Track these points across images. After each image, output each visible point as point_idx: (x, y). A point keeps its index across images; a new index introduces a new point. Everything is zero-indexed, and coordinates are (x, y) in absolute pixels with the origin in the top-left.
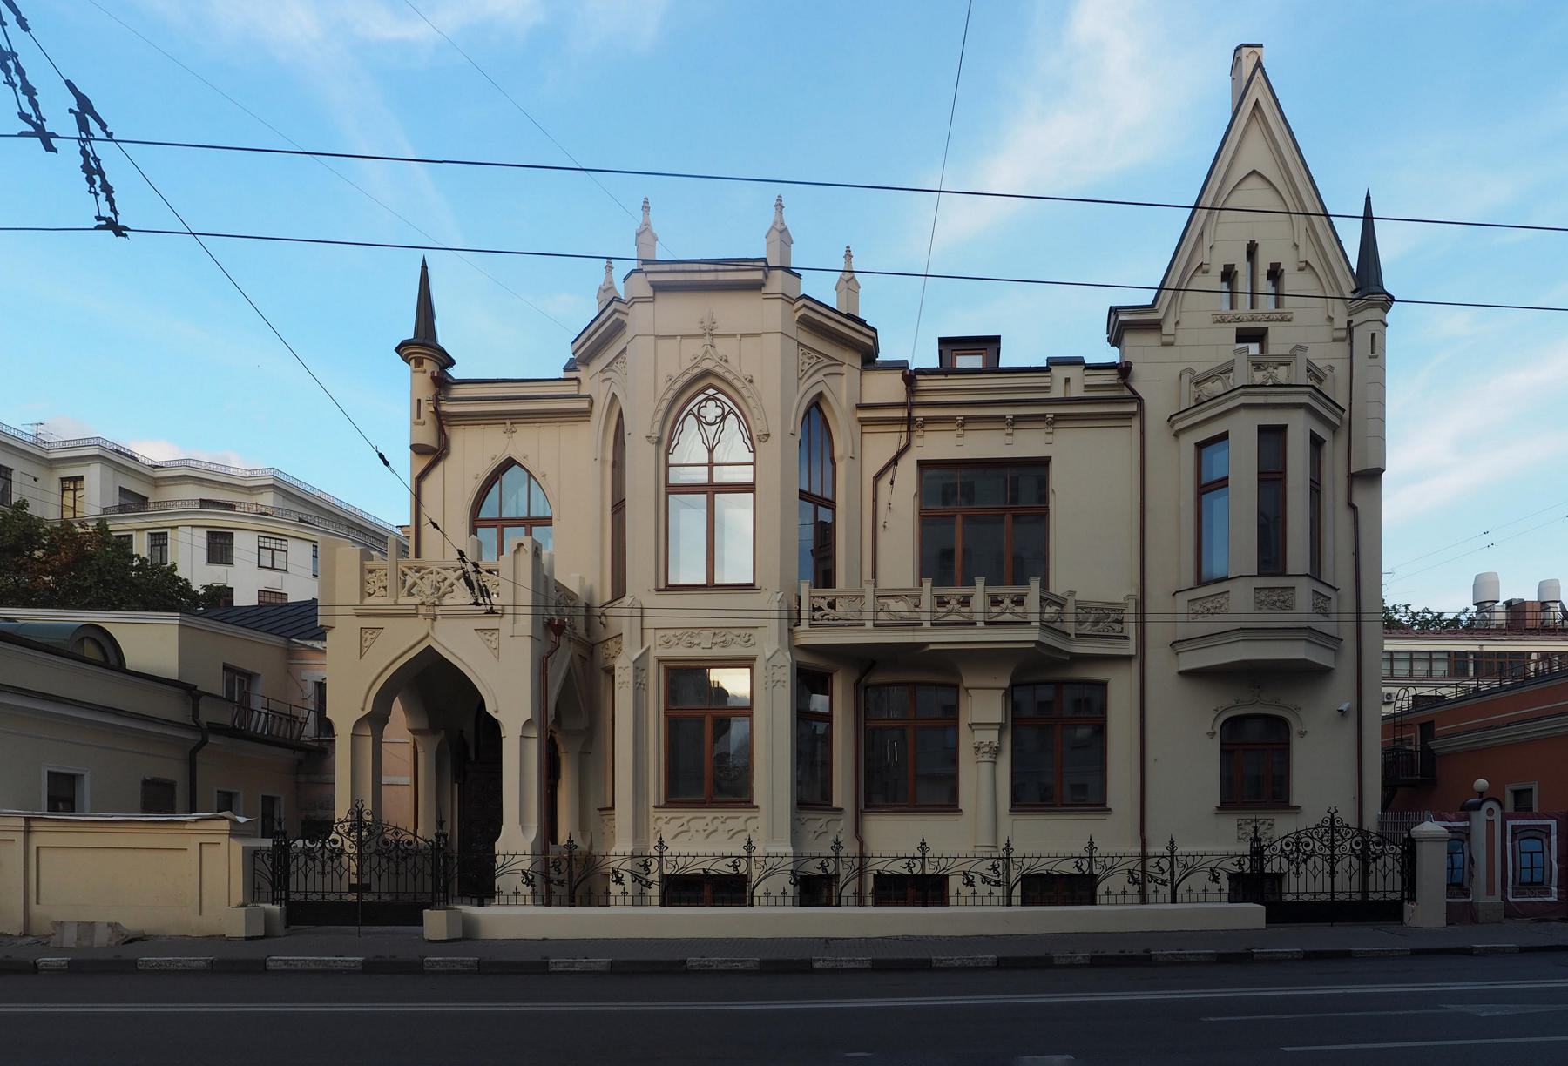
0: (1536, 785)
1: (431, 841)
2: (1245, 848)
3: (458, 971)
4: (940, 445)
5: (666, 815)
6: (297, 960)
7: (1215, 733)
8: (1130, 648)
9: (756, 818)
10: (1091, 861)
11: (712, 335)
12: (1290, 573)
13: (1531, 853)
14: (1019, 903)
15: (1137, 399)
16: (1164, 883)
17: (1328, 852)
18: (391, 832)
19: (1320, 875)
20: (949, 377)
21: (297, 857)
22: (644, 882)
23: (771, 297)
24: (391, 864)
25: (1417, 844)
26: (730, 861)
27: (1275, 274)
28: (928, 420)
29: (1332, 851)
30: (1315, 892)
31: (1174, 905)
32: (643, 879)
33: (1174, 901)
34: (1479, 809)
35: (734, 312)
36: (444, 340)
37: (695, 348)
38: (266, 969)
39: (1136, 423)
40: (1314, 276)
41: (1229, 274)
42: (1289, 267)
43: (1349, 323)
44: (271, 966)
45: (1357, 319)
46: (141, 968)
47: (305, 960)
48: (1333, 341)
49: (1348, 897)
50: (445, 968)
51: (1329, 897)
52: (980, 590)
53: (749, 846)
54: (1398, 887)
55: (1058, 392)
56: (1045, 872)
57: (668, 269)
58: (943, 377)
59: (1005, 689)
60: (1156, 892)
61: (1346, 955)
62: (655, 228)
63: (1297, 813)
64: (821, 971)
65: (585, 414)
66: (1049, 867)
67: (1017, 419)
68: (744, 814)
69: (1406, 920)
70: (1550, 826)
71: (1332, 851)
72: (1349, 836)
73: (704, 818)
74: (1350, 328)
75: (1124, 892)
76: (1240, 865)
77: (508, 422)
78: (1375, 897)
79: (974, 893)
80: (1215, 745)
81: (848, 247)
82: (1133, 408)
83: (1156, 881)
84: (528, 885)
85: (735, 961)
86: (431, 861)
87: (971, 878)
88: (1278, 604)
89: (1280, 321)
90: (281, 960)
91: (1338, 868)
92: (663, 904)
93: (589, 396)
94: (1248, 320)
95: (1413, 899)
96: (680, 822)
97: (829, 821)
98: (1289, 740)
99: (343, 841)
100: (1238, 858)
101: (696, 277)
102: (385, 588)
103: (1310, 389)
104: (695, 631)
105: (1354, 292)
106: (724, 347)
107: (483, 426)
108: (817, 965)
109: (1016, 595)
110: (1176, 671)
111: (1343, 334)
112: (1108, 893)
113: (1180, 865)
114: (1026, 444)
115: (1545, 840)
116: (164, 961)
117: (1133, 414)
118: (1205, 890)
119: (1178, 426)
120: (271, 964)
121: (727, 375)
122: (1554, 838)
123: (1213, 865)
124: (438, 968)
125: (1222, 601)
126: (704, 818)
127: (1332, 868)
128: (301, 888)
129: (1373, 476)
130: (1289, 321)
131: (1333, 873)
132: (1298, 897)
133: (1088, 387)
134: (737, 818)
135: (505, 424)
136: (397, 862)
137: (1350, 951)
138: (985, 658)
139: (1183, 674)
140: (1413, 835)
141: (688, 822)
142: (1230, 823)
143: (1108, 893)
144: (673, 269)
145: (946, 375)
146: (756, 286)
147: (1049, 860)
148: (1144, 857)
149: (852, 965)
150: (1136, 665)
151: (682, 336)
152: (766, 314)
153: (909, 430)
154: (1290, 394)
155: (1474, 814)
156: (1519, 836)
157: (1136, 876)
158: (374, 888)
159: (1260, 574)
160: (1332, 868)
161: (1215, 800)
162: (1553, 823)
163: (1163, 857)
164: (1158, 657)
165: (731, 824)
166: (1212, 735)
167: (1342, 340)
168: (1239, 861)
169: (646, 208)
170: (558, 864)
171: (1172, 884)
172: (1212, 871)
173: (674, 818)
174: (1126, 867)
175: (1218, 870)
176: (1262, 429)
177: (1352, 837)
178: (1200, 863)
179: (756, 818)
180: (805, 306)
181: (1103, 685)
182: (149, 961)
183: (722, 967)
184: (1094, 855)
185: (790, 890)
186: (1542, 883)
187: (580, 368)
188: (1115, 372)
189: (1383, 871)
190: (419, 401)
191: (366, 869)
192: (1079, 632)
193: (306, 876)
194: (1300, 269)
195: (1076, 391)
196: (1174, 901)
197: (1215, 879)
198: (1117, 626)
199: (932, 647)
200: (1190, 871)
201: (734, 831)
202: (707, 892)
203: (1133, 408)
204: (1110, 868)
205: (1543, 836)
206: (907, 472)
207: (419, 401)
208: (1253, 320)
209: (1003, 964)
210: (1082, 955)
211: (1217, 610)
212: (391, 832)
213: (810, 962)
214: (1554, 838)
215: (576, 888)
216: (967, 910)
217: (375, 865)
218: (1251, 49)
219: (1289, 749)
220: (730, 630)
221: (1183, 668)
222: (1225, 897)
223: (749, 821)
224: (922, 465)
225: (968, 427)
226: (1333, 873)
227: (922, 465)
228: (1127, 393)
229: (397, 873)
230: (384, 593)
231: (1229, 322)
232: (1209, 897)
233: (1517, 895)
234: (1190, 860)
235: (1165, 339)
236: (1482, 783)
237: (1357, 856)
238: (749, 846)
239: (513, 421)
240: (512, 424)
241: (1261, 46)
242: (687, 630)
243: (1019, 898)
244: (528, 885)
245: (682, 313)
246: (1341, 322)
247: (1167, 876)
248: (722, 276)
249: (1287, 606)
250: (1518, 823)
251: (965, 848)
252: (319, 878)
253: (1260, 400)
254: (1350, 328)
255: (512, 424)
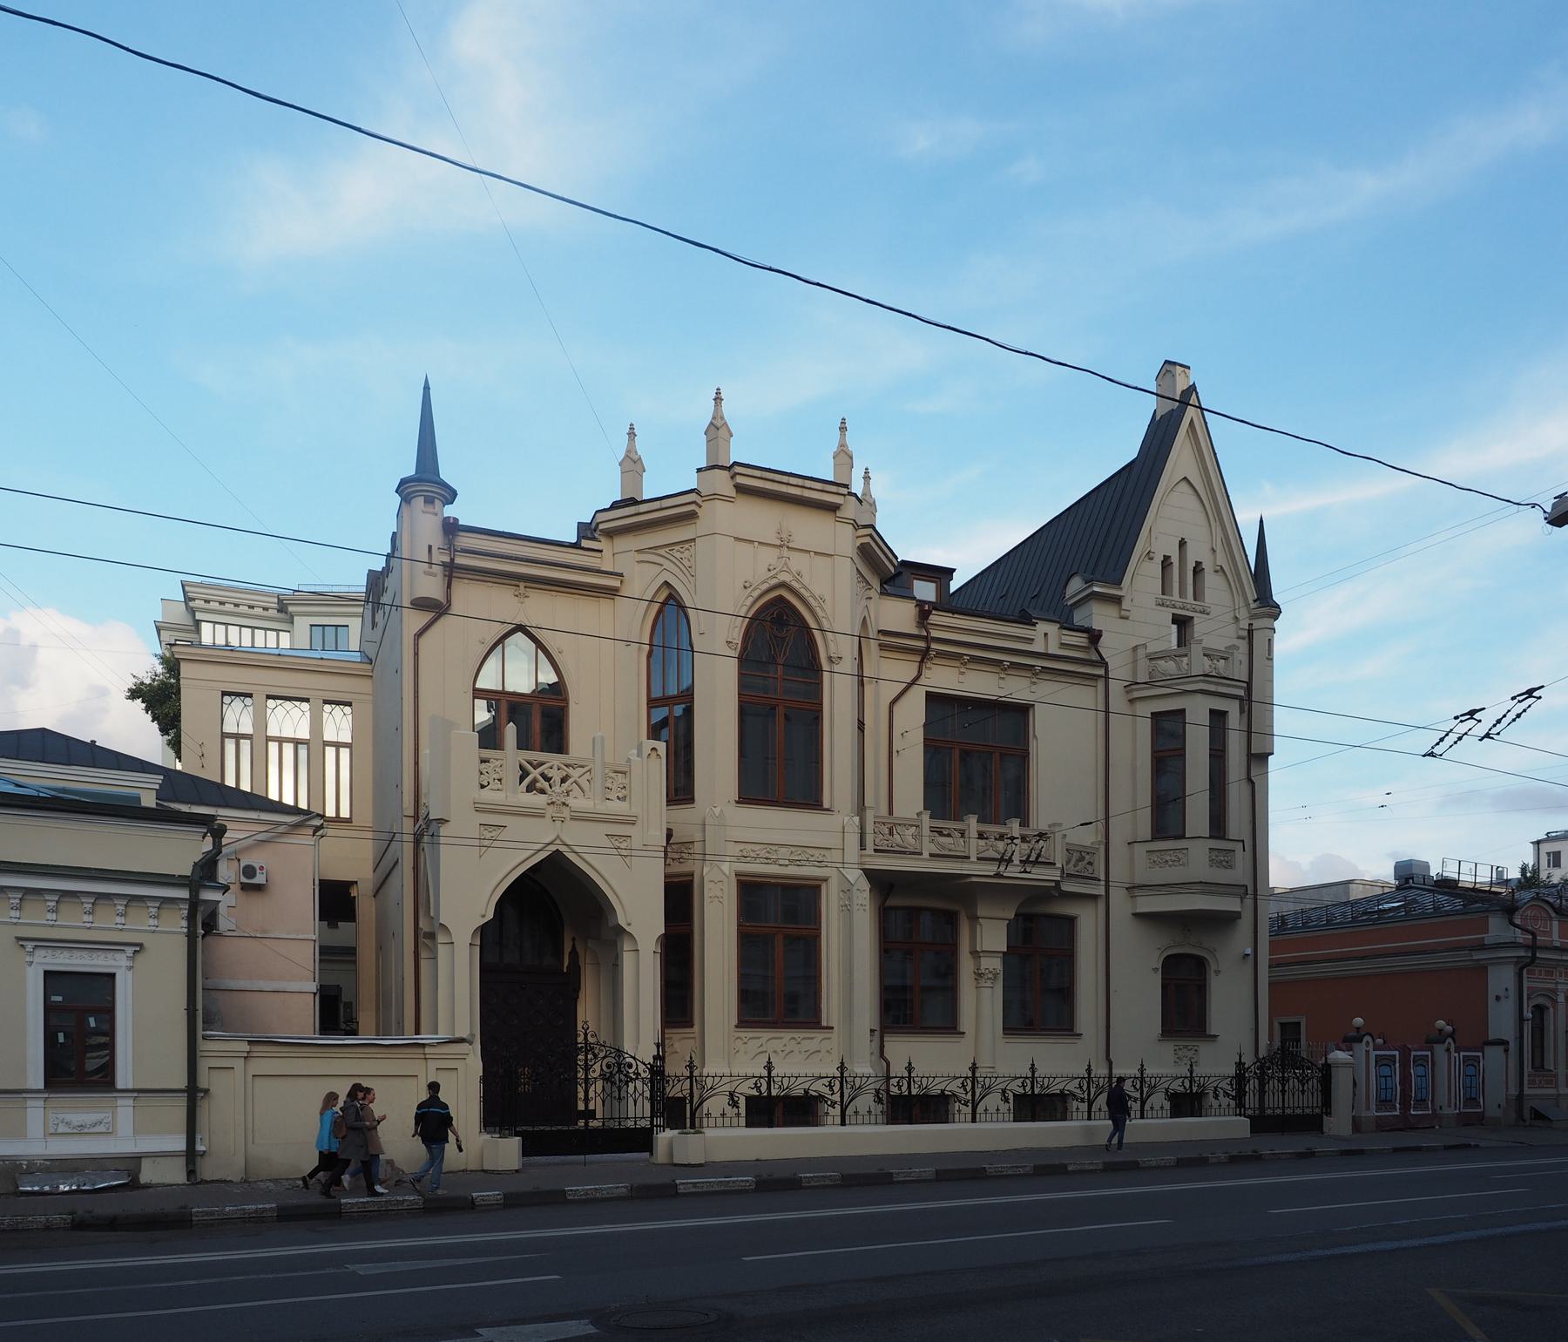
0: (1305, 1019)
1: (649, 1064)
2: (1232, 1071)
3: (827, 1185)
4: (944, 678)
5: (798, 1035)
6: (703, 1183)
7: (1158, 969)
8: (1101, 891)
9: (829, 1039)
10: (910, 1080)
11: (788, 547)
12: (1231, 838)
13: (1386, 1077)
14: (1012, 1119)
15: (1103, 663)
16: (1083, 1100)
17: (1281, 1075)
18: (613, 1055)
19: (1276, 1094)
20: (956, 616)
21: (1249, 1081)
22: (829, 1103)
23: (844, 520)
24: (615, 1089)
25: (1332, 1069)
26: (826, 1081)
27: (1198, 569)
28: (941, 654)
29: (1283, 1074)
30: (635, 1118)
31: (843, 1127)
32: (828, 1099)
33: (843, 1123)
34: (1361, 1041)
35: (808, 528)
36: (445, 474)
37: (769, 556)
38: (677, 1193)
39: (1101, 684)
40: (1224, 577)
41: (1166, 563)
42: (1208, 566)
43: (1251, 625)
44: (681, 1189)
45: (1257, 624)
46: (569, 1198)
47: (710, 1182)
48: (1238, 638)
49: (601, 1124)
50: (818, 1184)
51: (649, 1123)
52: (972, 824)
53: (769, 1067)
54: (648, 1113)
55: (1038, 647)
56: (1058, 1092)
57: (759, 475)
58: (951, 615)
59: (1009, 920)
60: (959, 1111)
61: (1418, 1149)
62: (851, 447)
63: (1214, 1041)
64: (1074, 1172)
65: (612, 592)
66: (942, 1086)
67: (1014, 665)
68: (818, 1035)
69: (1325, 1129)
70: (1395, 1056)
71: (1283, 1074)
72: (602, 1055)
73: (759, 1038)
74: (1250, 632)
75: (723, 1115)
76: (758, 1089)
77: (522, 585)
78: (1269, 1112)
79: (1220, 1105)
80: (1157, 979)
81: (867, 469)
82: (1101, 672)
83: (960, 1102)
84: (733, 1107)
85: (1017, 1167)
86: (583, 1085)
87: (736, 1099)
88: (1224, 863)
89: (1201, 613)
90: (690, 1183)
91: (1286, 1088)
92: (748, 1125)
93: (621, 575)
94: (1180, 608)
95: (1329, 1114)
96: (758, 1042)
97: (823, 1039)
98: (1205, 978)
99: (637, 1065)
100: (897, 1080)
101: (784, 489)
102: (500, 780)
103: (852, 522)
104: (774, 848)
105: (1255, 601)
106: (798, 562)
107: (490, 584)
108: (1070, 1169)
109: (999, 833)
110: (1131, 912)
111: (1245, 633)
112: (856, 1112)
113: (777, 1086)
114: (1014, 689)
115: (1393, 1067)
116: (591, 1189)
117: (1099, 676)
118: (998, 1110)
119: (1136, 694)
120: (681, 1187)
121: (803, 591)
122: (1397, 1065)
123: (1002, 1086)
124: (812, 1183)
125: (1180, 856)
126: (781, 1038)
127: (1283, 1088)
128: (1310, 1105)
129: (1263, 757)
130: (1208, 614)
131: (1283, 1092)
132: (635, 1122)
133: (1063, 645)
134: (812, 1038)
135: (518, 586)
136: (620, 1086)
137: (1363, 1150)
138: (996, 891)
139: (1137, 915)
140: (1329, 1062)
141: (750, 1039)
142: (1169, 1048)
143: (1152, 1108)
144: (764, 476)
145: (953, 613)
146: (833, 508)
147: (1215, 1079)
148: (1110, 1077)
149: (1091, 1167)
150: (1101, 905)
151: (759, 543)
152: (845, 541)
153: (921, 662)
154: (1229, 686)
155: (1355, 1046)
156: (1379, 1064)
157: (881, 1096)
158: (599, 1115)
159: (1211, 837)
160: (1283, 1088)
161: (1157, 1028)
162: (1397, 1053)
163: (1027, 1078)
164: (1118, 896)
165: (807, 1045)
166: (1155, 970)
167: (1243, 638)
168: (830, 1082)
169: (843, 429)
170: (759, 1085)
171: (842, 1105)
172: (731, 1095)
173: (804, 1039)
174: (872, 1086)
175: (737, 1095)
176: (1212, 712)
177: (604, 1058)
178: (933, 1084)
179: (829, 1039)
180: (871, 536)
181: (1071, 921)
182: (578, 1190)
183: (1010, 1172)
184: (772, 1075)
185: (1167, 1105)
186: (1391, 1101)
187: (602, 539)
188: (1085, 635)
189: (601, 1095)
190: (430, 547)
191: (591, 1094)
192: (980, 856)
193: (1293, 1095)
194: (1216, 571)
195: (1054, 649)
196: (974, 1120)
197: (735, 1104)
198: (1089, 867)
199: (974, 879)
200: (987, 1090)
201: (811, 1051)
202: (779, 1112)
203: (1101, 672)
204: (711, 1088)
205: (1391, 1064)
206: (916, 700)
207: (430, 547)
208: (1183, 608)
209: (1181, 1163)
210: (492, 1195)
211: (1175, 863)
212: (613, 1055)
213: (1065, 1166)
214: (1397, 1065)
215: (847, 1107)
216: (1160, 1121)
217: (599, 1090)
218: (1183, 369)
219: (1205, 985)
220: (806, 849)
221: (1139, 910)
222: (743, 1121)
223: (770, 1042)
224: (932, 698)
225: (970, 666)
226: (1283, 1092)
227: (932, 698)
228: (1095, 657)
229: (620, 1098)
230: (500, 786)
231: (1167, 606)
232: (727, 1122)
233: (1417, 1108)
234: (786, 1081)
235: (1123, 613)
236: (1359, 1021)
237: (1298, 1078)
238: (769, 1067)
239: (528, 584)
240: (525, 587)
241: (1189, 368)
242: (766, 846)
243: (1169, 1112)
244: (733, 1107)
245: (762, 519)
246: (1244, 624)
247: (969, 1097)
248: (807, 493)
249: (1229, 865)
250: (1419, 1053)
251: (1003, 1070)
252: (616, 1103)
253: (1212, 688)
254: (1250, 632)
255: (525, 587)
